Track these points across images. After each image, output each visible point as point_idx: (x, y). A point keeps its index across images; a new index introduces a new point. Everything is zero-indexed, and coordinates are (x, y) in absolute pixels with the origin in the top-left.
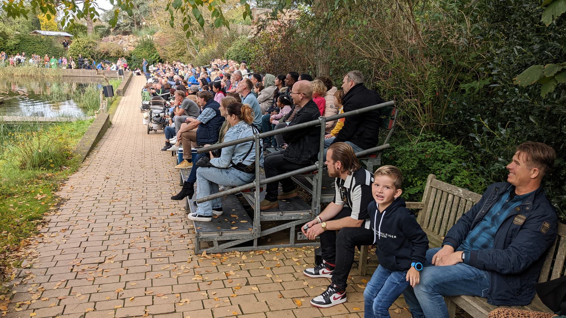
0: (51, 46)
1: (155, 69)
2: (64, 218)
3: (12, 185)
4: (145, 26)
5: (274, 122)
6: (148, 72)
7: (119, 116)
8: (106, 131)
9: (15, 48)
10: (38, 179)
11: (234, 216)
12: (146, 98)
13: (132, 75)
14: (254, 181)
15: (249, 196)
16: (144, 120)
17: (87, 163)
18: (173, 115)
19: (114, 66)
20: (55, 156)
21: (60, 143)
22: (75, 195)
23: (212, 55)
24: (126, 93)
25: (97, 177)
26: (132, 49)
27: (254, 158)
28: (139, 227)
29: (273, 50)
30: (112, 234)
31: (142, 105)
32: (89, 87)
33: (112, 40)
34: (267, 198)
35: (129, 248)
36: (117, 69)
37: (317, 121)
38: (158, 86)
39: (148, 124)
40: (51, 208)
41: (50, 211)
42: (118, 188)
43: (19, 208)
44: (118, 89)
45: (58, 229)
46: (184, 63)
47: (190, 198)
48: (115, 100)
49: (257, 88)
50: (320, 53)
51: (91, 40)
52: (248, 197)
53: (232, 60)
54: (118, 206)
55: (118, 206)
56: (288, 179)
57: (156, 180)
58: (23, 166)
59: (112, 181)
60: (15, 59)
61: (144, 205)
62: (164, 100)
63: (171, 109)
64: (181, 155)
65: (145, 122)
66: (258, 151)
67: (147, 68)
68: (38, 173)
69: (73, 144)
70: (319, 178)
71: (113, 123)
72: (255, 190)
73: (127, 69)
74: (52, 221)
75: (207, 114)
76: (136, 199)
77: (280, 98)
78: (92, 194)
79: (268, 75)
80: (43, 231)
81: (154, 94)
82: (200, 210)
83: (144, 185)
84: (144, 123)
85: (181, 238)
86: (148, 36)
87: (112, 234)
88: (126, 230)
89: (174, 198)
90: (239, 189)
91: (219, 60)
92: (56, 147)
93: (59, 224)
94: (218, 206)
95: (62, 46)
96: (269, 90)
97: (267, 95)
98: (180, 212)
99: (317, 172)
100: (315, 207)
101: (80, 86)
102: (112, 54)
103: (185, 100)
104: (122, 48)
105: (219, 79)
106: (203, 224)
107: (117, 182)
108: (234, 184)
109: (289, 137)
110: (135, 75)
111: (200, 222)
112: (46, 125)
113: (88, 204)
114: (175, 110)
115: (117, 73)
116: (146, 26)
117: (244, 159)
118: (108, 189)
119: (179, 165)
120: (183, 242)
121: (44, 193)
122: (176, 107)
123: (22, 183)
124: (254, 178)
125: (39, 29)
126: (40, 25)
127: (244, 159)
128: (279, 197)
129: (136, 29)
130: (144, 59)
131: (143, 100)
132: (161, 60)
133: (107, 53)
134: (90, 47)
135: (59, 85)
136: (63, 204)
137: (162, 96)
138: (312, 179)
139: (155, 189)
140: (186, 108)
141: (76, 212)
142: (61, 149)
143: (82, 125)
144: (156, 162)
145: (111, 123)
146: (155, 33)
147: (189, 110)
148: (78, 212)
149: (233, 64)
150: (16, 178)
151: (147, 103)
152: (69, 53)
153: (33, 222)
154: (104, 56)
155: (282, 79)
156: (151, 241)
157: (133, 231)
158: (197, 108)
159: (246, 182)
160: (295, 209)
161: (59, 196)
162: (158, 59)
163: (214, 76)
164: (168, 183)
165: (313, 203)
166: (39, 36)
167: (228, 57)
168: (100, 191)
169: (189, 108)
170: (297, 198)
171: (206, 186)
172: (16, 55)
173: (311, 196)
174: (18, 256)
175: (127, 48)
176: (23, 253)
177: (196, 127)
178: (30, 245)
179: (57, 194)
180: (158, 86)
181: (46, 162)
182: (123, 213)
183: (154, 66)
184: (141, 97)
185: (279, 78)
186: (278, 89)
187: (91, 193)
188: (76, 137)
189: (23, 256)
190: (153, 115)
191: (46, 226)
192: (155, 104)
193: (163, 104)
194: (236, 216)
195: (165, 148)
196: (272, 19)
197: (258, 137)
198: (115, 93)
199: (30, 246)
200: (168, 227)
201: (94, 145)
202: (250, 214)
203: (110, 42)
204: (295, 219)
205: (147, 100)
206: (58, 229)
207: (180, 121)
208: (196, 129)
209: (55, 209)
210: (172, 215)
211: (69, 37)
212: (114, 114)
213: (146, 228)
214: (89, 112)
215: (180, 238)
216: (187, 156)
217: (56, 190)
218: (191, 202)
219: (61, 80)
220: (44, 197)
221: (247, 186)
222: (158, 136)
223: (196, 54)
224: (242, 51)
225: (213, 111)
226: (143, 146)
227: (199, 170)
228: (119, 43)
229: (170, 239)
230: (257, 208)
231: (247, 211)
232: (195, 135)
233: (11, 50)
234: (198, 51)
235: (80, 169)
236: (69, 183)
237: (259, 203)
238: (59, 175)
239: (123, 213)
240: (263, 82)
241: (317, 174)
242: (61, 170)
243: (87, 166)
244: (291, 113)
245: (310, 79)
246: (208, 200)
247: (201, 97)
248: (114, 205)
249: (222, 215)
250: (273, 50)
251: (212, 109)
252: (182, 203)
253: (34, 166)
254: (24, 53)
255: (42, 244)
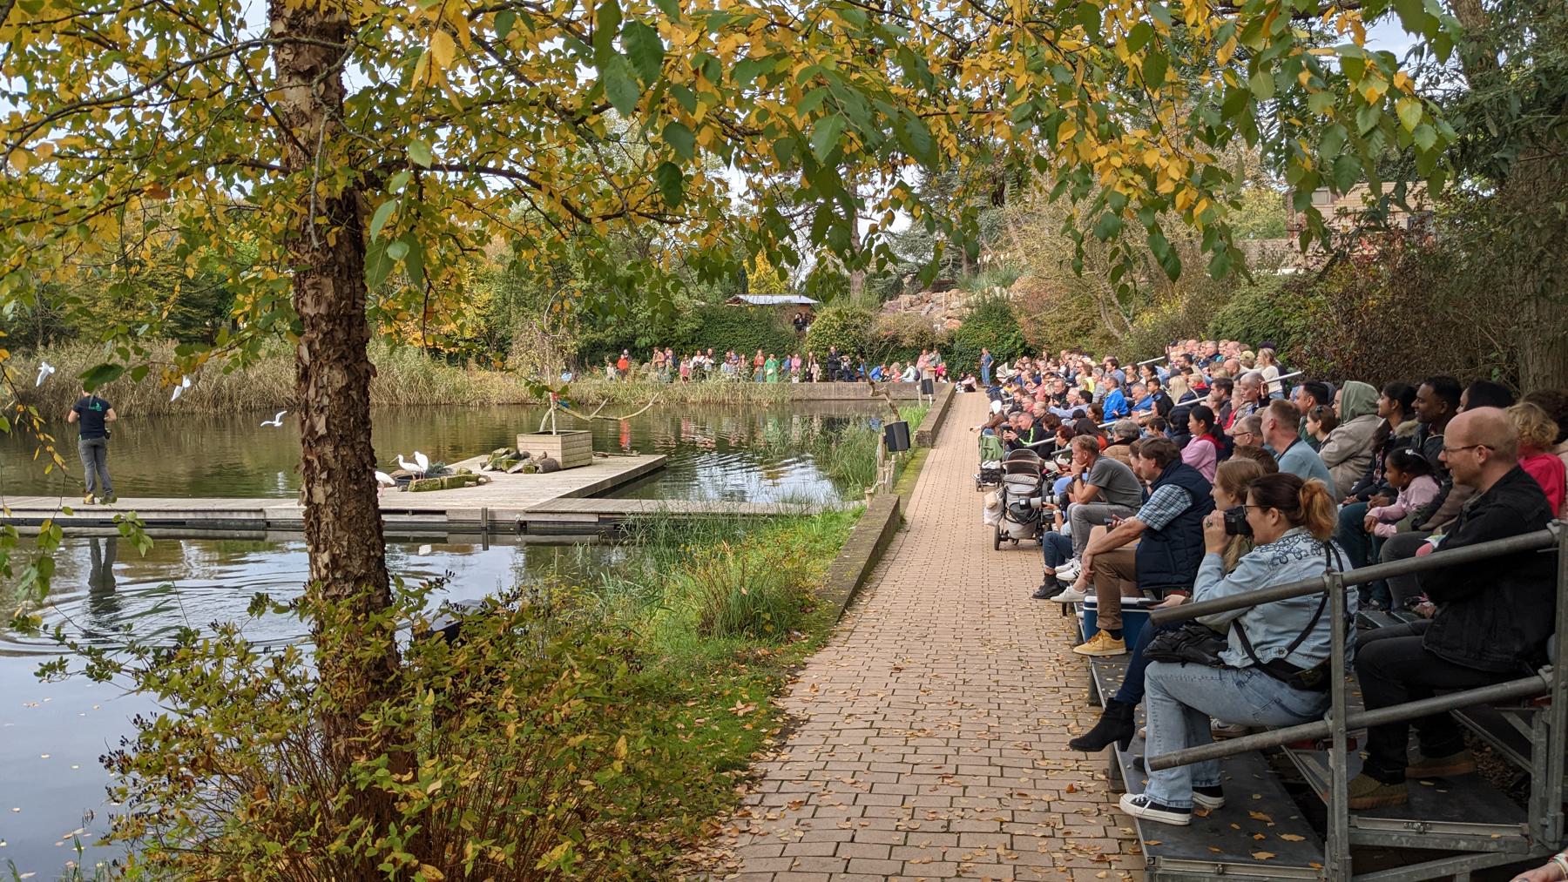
0: (769, 330)
1: (1011, 373)
2: (796, 770)
3: (682, 673)
4: (990, 265)
5: (1379, 529)
6: (995, 381)
7: (923, 501)
8: (891, 540)
9: (693, 340)
10: (738, 661)
11: (1260, 816)
12: (990, 452)
13: (955, 390)
14: (1326, 717)
15: (1311, 762)
16: (986, 512)
17: (848, 624)
18: (1065, 502)
19: (911, 370)
20: (776, 603)
21: (786, 573)
22: (822, 710)
23: (1172, 330)
24: (939, 439)
25: (872, 664)
26: (955, 325)
27: (1327, 647)
28: (985, 817)
29: (1367, 309)
30: (913, 830)
31: (979, 472)
32: (851, 426)
33: (908, 305)
34: (1369, 769)
35: (958, 876)
36: (917, 379)
37: (1542, 535)
38: (1025, 421)
39: (995, 523)
40: (768, 742)
41: (765, 748)
42: (924, 699)
43: (697, 734)
44: (920, 429)
45: (785, 800)
46: (1091, 355)
47: (1124, 748)
48: (913, 457)
49: (1316, 421)
50: (1530, 312)
51: (859, 309)
52: (1308, 764)
53: (1231, 340)
54: (928, 750)
55: (928, 750)
56: (1441, 719)
57: (1022, 684)
58: (706, 627)
59: (908, 678)
60: (691, 365)
61: (994, 753)
62: (1038, 460)
63: (1059, 486)
64: (1091, 617)
65: (988, 517)
66: (1340, 626)
67: (993, 371)
68: (740, 645)
69: (819, 573)
70: (1554, 720)
71: (909, 519)
72: (1330, 745)
73: (940, 379)
74: (770, 776)
75: (1163, 502)
76: (971, 735)
77: (1392, 457)
78: (863, 711)
79: (1352, 385)
80: (749, 802)
81: (1013, 445)
82: (1156, 787)
83: (991, 694)
84: (987, 520)
85: (1101, 865)
86: (997, 289)
87: (913, 830)
88: (949, 821)
89: (1082, 744)
90: (1279, 735)
91: (1192, 342)
92: (779, 582)
93: (786, 787)
94: (1209, 781)
95: (792, 329)
96: (1358, 429)
97: (1348, 443)
98: (1092, 784)
99: (1549, 701)
100: (1543, 815)
101: (831, 423)
102: (907, 342)
103: (1099, 462)
104: (931, 324)
105: (1194, 397)
106: (1164, 832)
107: (921, 680)
108: (1260, 721)
109: (1437, 580)
110: (961, 390)
111: (1156, 824)
112: (757, 522)
113: (852, 737)
114: (1070, 488)
115: (918, 388)
116: (991, 265)
117: (1291, 648)
118: (900, 698)
119: (1086, 645)
120: (1107, 876)
121: (752, 700)
122: (1074, 480)
123: (703, 671)
124: (1326, 704)
125: (745, 292)
126: (746, 282)
127: (1291, 648)
128: (1409, 771)
129: (965, 273)
130: (984, 350)
131: (984, 458)
132: (1030, 349)
133: (895, 340)
134: (856, 327)
135: (781, 420)
136: (793, 732)
137: (1036, 448)
138: (1530, 725)
139: (1020, 708)
140: (1102, 483)
141: (824, 757)
142: (788, 586)
143: (834, 522)
144: (1020, 629)
145: (903, 520)
146: (1013, 281)
147: (1112, 487)
148: (828, 759)
149: (1232, 352)
150: (691, 657)
151: (994, 465)
152: (808, 345)
153: (726, 774)
154: (887, 346)
155: (1404, 401)
156: (1015, 862)
157: (966, 826)
158: (1134, 482)
159: (1300, 716)
160: (1470, 817)
161: (783, 711)
162: (1021, 346)
163: (1177, 390)
164: (1053, 695)
165: (1534, 802)
166: (744, 307)
167: (1218, 333)
168: (881, 704)
169: (1110, 482)
170: (1473, 778)
171: (1175, 721)
172: (693, 355)
173: (1528, 777)
174: (694, 863)
175: (942, 323)
176: (704, 856)
177: (1135, 538)
178: (721, 835)
179: (780, 703)
180: (1025, 421)
181: (755, 619)
182: (939, 771)
183: (1011, 367)
184: (978, 450)
185: (1392, 394)
186: (1387, 427)
187: (858, 709)
188: (822, 554)
189: (706, 863)
190: (1011, 500)
191: (756, 788)
192: (1015, 469)
193: (1037, 470)
194: (1267, 818)
195: (1043, 593)
196: (1369, 228)
197: (1339, 581)
198: (913, 440)
199: (720, 840)
200: (1061, 826)
201: (865, 578)
202: (1314, 817)
203: (903, 311)
204: (1471, 848)
205: (992, 459)
206: (785, 800)
207: (1085, 518)
208: (1133, 545)
209: (775, 744)
210: (1072, 790)
211: (808, 305)
212: (910, 493)
213: (1002, 823)
214: (851, 492)
215: (1096, 865)
216: (1110, 622)
217: (779, 694)
218: (1125, 760)
219: (787, 409)
220: (751, 709)
221: (1305, 729)
222: (1023, 556)
223: (1124, 329)
224: (1263, 314)
225: (1182, 494)
226: (985, 584)
227: (1152, 669)
228: (923, 313)
229: (1069, 864)
230: (1337, 803)
231: (1298, 803)
232: (1133, 561)
233: (684, 344)
234: (1132, 322)
235: (831, 640)
236: (809, 676)
237: (1344, 784)
238: (784, 654)
239: (939, 771)
240: (1337, 407)
241: (1547, 708)
242: (789, 641)
243: (847, 634)
244: (1438, 501)
245: (1501, 397)
246: (1182, 763)
247: (1148, 457)
248: (917, 748)
249: (1222, 808)
250: (1367, 309)
251: (1179, 489)
252: (1099, 760)
253: (730, 629)
254: (710, 351)
255: (747, 838)
